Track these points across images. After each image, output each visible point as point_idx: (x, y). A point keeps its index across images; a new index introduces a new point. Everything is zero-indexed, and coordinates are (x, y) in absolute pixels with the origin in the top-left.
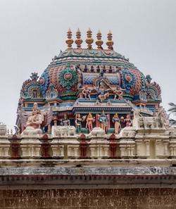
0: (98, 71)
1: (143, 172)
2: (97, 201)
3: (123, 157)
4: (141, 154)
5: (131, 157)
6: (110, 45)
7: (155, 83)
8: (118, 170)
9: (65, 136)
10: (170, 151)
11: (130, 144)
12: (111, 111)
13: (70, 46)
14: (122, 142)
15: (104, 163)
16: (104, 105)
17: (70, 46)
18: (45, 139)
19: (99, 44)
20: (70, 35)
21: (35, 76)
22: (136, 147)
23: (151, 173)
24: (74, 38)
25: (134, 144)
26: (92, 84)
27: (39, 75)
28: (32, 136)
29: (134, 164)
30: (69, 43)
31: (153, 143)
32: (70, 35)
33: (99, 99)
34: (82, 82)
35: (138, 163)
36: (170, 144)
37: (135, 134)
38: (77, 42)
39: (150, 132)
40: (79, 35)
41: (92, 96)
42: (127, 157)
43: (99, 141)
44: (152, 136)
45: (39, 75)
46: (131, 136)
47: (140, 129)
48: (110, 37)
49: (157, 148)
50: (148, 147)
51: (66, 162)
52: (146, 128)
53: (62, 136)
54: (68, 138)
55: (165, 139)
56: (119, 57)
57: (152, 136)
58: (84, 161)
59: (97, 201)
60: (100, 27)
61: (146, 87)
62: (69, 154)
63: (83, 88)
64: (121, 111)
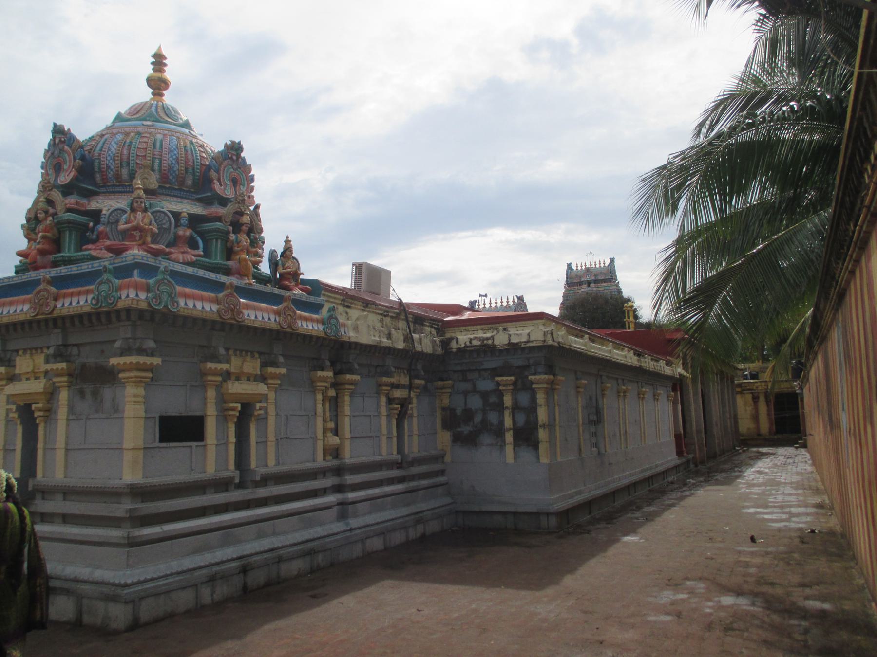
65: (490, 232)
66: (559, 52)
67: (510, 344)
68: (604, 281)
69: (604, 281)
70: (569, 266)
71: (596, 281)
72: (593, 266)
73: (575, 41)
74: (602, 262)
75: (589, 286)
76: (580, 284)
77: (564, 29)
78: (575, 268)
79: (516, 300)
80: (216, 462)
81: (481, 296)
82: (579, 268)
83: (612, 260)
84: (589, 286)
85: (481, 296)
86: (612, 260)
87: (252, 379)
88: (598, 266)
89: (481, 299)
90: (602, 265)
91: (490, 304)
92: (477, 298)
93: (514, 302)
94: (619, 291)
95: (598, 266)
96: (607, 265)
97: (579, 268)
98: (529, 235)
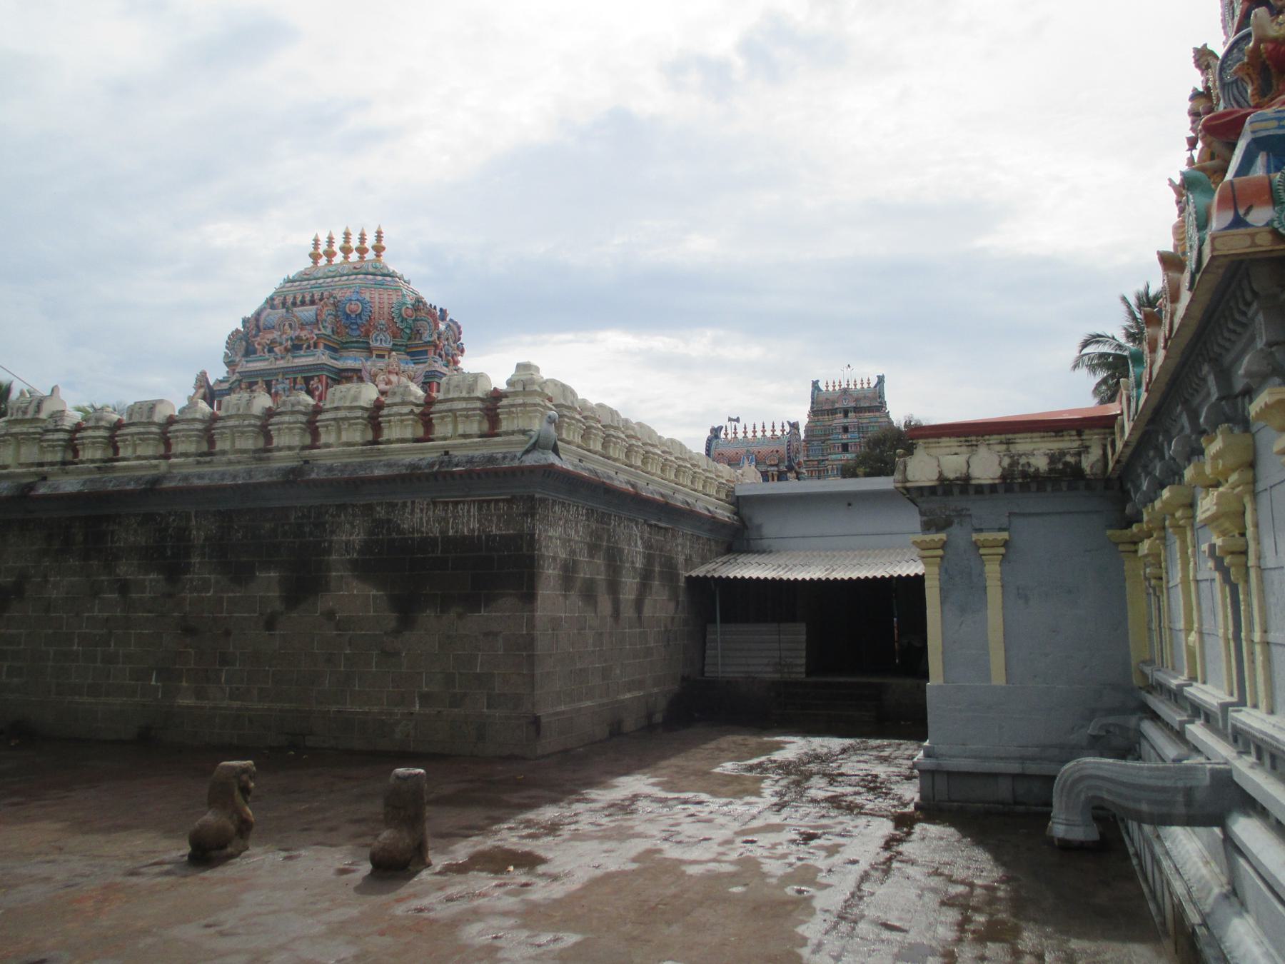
0: (284, 304)
6: (379, 249)
8: (496, 447)
12: (250, 376)
13: (315, 262)
16: (281, 364)
17: (315, 262)
18: (430, 402)
19: (362, 251)
24: (355, 243)
30: (315, 257)
38: (358, 250)
40: (362, 239)
43: (341, 414)
48: (379, 236)
60: (365, 223)
64: (309, 371)
65: (601, 335)
66: (716, 76)
67: (942, 478)
68: (870, 409)
69: (870, 409)
70: (815, 385)
71: (857, 410)
72: (852, 386)
73: (739, 62)
74: (865, 381)
75: (846, 415)
76: (833, 412)
77: (723, 43)
78: (824, 389)
79: (787, 428)
80: (1003, 608)
81: (730, 420)
82: (831, 389)
83: (881, 380)
84: (846, 415)
85: (730, 420)
86: (881, 380)
87: (956, 491)
88: (859, 387)
89: (730, 426)
90: (865, 386)
91: (745, 433)
92: (723, 422)
93: (783, 431)
94: (891, 423)
95: (859, 387)
96: (872, 385)
97: (831, 389)
98: (660, 343)
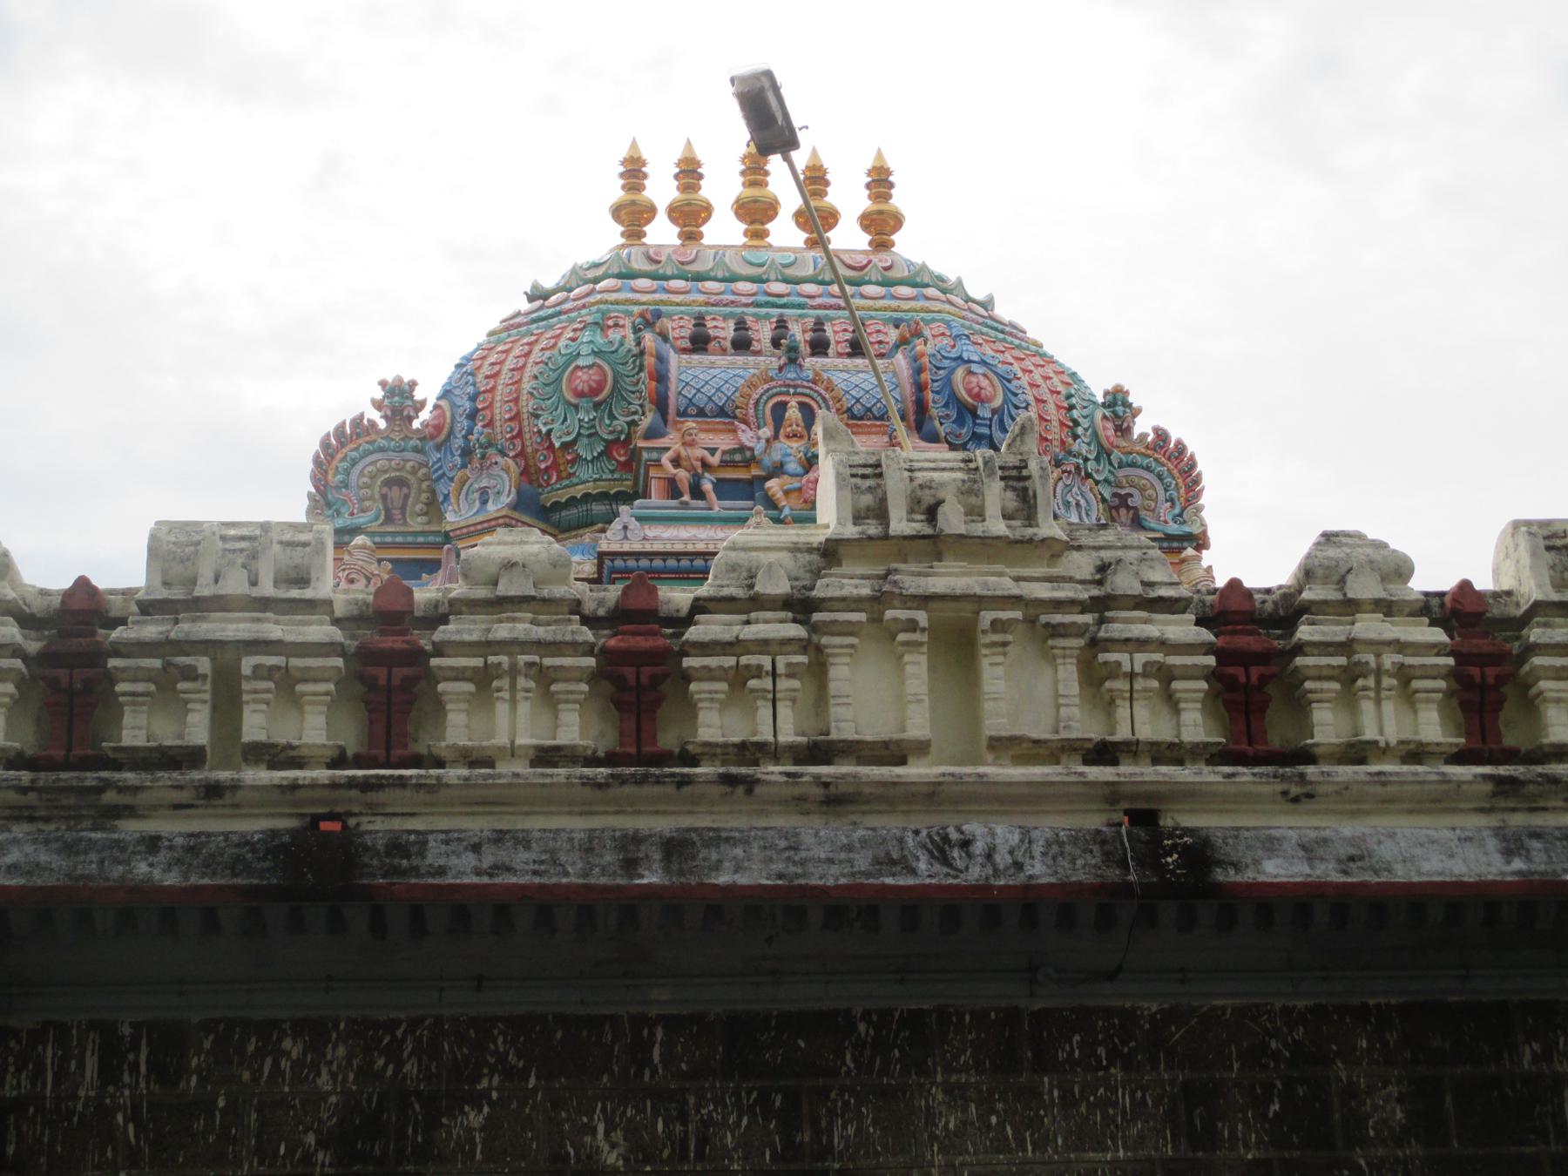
1: (862, 861)
2: (475, 1119)
3: (712, 751)
4: (847, 724)
5: (771, 751)
6: (881, 224)
7: (1162, 436)
9: (236, 585)
10: (1109, 706)
11: (763, 645)
13: (634, 233)
14: (706, 629)
15: (544, 800)
17: (634, 233)
20: (634, 172)
21: (398, 399)
22: (818, 669)
23: (926, 871)
24: (661, 189)
25: (804, 646)
26: (725, 414)
27: (428, 391)
28: (140, 699)
29: (799, 803)
30: (633, 216)
31: (957, 638)
32: (634, 172)
33: (771, 503)
34: (661, 404)
35: (835, 800)
36: (1095, 644)
37: (817, 574)
39: (933, 545)
41: (726, 489)
42: (751, 752)
44: (950, 578)
45: (428, 391)
46: (782, 587)
47: (851, 531)
48: (880, 182)
49: (995, 675)
50: (917, 667)
51: (213, 791)
52: (900, 524)
53: (204, 590)
54: (265, 604)
55: (1058, 605)
56: (919, 279)
57: (950, 578)
58: (366, 786)
59: (475, 1119)
61: (1104, 453)
62: (255, 725)
63: (672, 440)
